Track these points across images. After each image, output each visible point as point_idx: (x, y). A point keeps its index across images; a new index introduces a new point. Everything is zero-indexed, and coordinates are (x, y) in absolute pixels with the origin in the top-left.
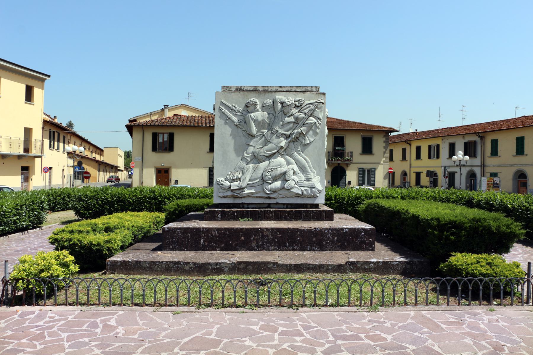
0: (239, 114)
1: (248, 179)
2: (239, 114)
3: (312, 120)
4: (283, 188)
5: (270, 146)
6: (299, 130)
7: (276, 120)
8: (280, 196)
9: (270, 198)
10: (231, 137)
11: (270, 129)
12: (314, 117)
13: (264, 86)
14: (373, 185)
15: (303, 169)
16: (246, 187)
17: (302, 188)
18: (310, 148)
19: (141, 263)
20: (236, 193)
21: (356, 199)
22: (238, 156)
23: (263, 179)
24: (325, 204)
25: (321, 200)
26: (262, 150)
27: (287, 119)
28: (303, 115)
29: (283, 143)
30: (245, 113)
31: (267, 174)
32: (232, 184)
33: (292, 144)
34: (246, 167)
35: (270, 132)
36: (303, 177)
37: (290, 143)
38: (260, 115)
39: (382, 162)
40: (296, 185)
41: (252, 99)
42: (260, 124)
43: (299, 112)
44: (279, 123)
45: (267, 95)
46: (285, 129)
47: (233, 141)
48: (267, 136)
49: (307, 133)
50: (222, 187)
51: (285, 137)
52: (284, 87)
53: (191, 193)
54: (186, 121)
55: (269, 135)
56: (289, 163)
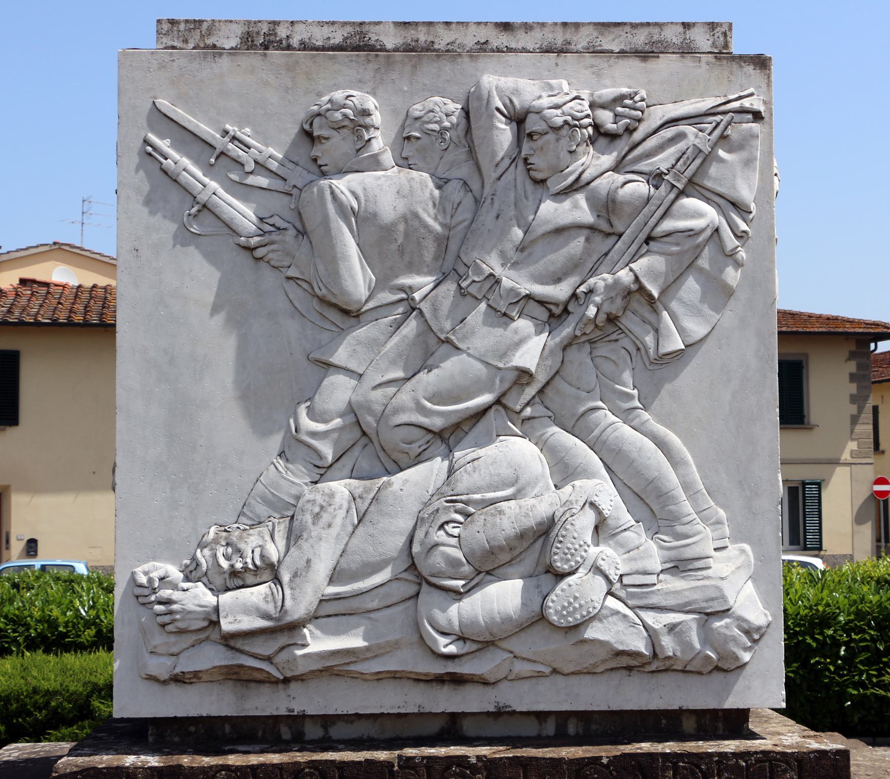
0: (262, 181)
1: (322, 568)
2: (262, 181)
3: (698, 213)
4: (539, 619)
5: (451, 368)
6: (625, 275)
7: (487, 217)
8: (522, 668)
9: (457, 680)
10: (220, 318)
11: (451, 265)
13: (405, 24)
14: (817, 548)
15: (651, 504)
16: (314, 617)
17: (650, 617)
18: (688, 380)
20: (253, 657)
21: (812, 625)
22: (261, 426)
24: (790, 712)
25: (762, 686)
26: (405, 397)
27: (553, 212)
28: (640, 187)
29: (531, 349)
30: (298, 177)
31: (441, 536)
32: (227, 598)
33: (580, 357)
34: (308, 494)
35: (449, 287)
36: (653, 555)
37: (573, 354)
38: (390, 188)
39: (846, 456)
40: (611, 602)
41: (339, 95)
42: (389, 244)
43: (616, 168)
44: (505, 232)
45: (429, 70)
46: (539, 267)
47: (230, 344)
48: (435, 310)
49: (670, 287)
50: (170, 622)
51: (543, 314)
52: (528, 27)
53: (56, 613)
54: (67, 304)
55: (446, 305)
56: (565, 471)
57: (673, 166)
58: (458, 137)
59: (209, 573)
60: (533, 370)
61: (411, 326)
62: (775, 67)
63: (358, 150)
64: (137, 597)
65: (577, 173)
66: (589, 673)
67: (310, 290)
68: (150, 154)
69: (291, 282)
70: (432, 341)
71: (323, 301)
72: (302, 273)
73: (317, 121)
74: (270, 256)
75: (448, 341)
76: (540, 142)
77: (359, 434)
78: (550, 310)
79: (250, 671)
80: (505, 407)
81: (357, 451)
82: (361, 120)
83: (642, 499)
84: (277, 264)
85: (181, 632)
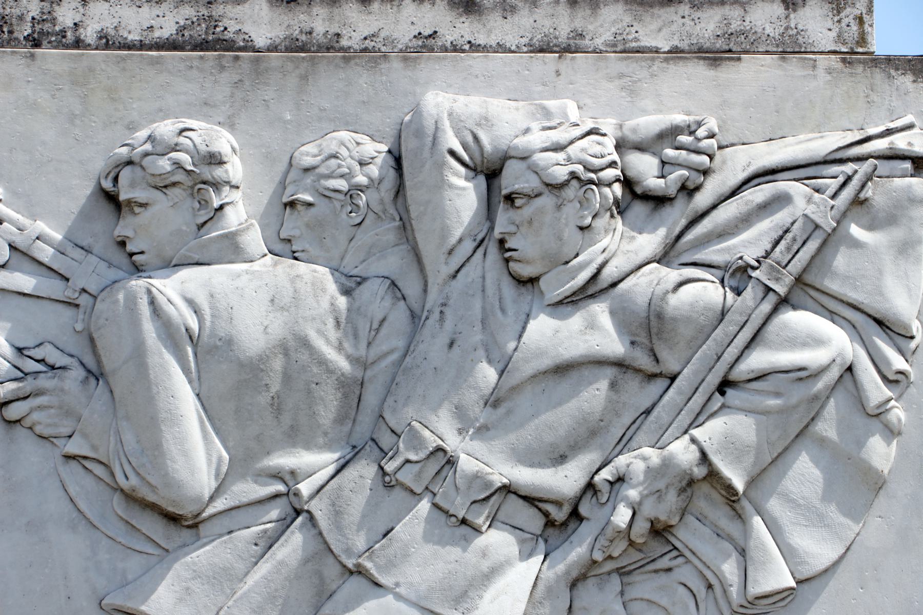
2: (24, 281)
3: (814, 339)
6: (682, 451)
7: (433, 344)
11: (366, 433)
12: (836, 308)
19: (197, 391)
27: (550, 335)
28: (709, 292)
30: (88, 273)
35: (364, 472)
37: (589, 594)
38: (258, 293)
41: (166, 128)
42: (254, 393)
43: (664, 257)
44: (464, 372)
45: (330, 84)
48: (337, 513)
51: (532, 520)
55: (357, 504)
57: (767, 255)
58: (382, 202)
69: (73, 464)
70: (331, 571)
73: (126, 175)
74: (35, 416)
75: (360, 571)
76: (527, 211)
78: (546, 514)
84: (46, 432)
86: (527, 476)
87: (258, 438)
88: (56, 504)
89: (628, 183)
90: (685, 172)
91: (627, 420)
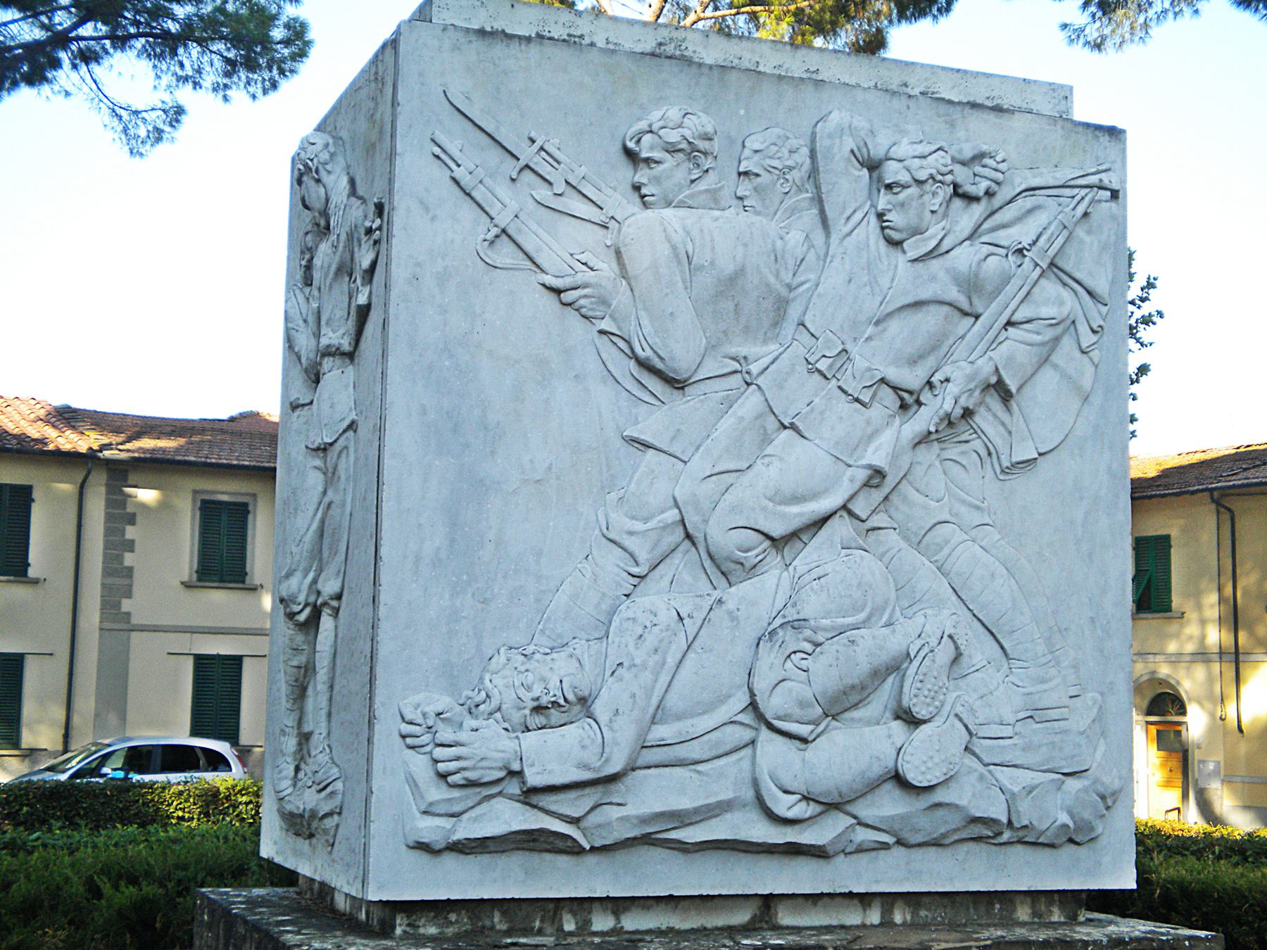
8: (863, 835)
17: (1003, 775)
23: (753, 705)
29: (887, 441)
33: (927, 455)
57: (1035, 242)
58: (801, 178)
59: (504, 707)
60: (887, 469)
61: (750, 403)
62: (1130, 138)
63: (693, 181)
64: (404, 737)
65: (939, 237)
66: (934, 845)
67: (627, 351)
68: (438, 157)
69: (605, 337)
70: (771, 423)
71: (644, 365)
72: (619, 328)
73: (647, 138)
74: (582, 302)
75: (793, 427)
76: (902, 196)
77: (682, 535)
78: (902, 399)
79: (552, 839)
80: (851, 513)
81: (677, 558)
82: (702, 145)
83: (992, 634)
84: (590, 314)
85: (471, 784)
86: (893, 374)
87: (725, 333)
88: (593, 366)
89: (956, 186)
90: (989, 183)
91: (951, 342)
